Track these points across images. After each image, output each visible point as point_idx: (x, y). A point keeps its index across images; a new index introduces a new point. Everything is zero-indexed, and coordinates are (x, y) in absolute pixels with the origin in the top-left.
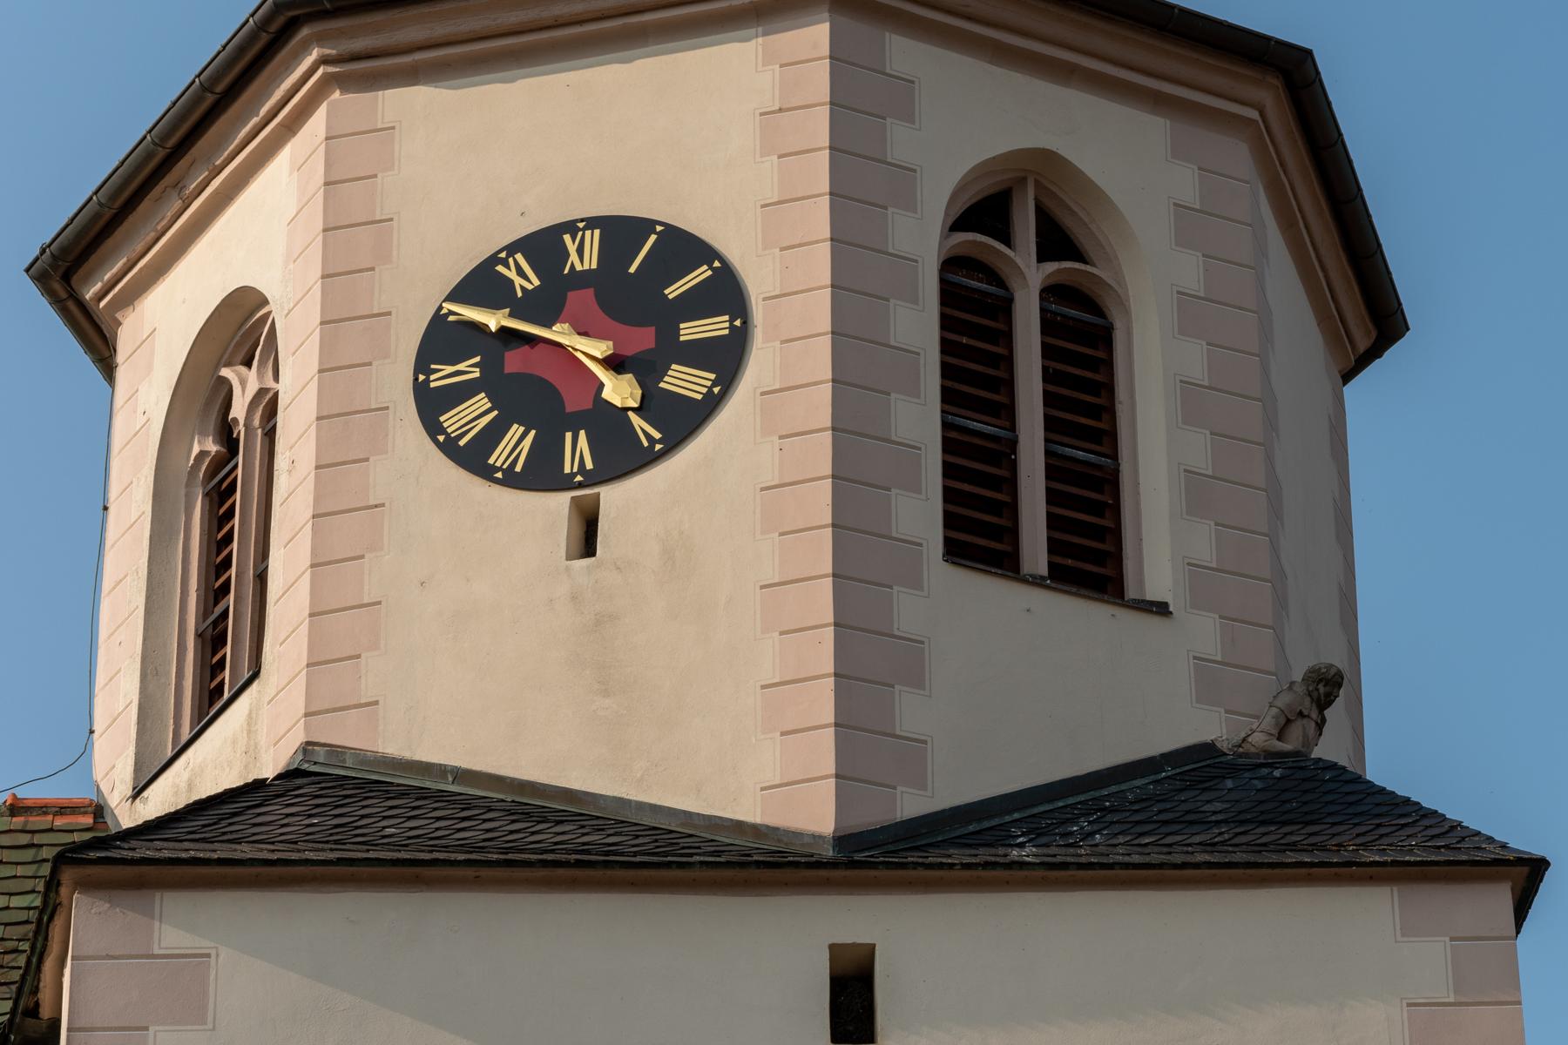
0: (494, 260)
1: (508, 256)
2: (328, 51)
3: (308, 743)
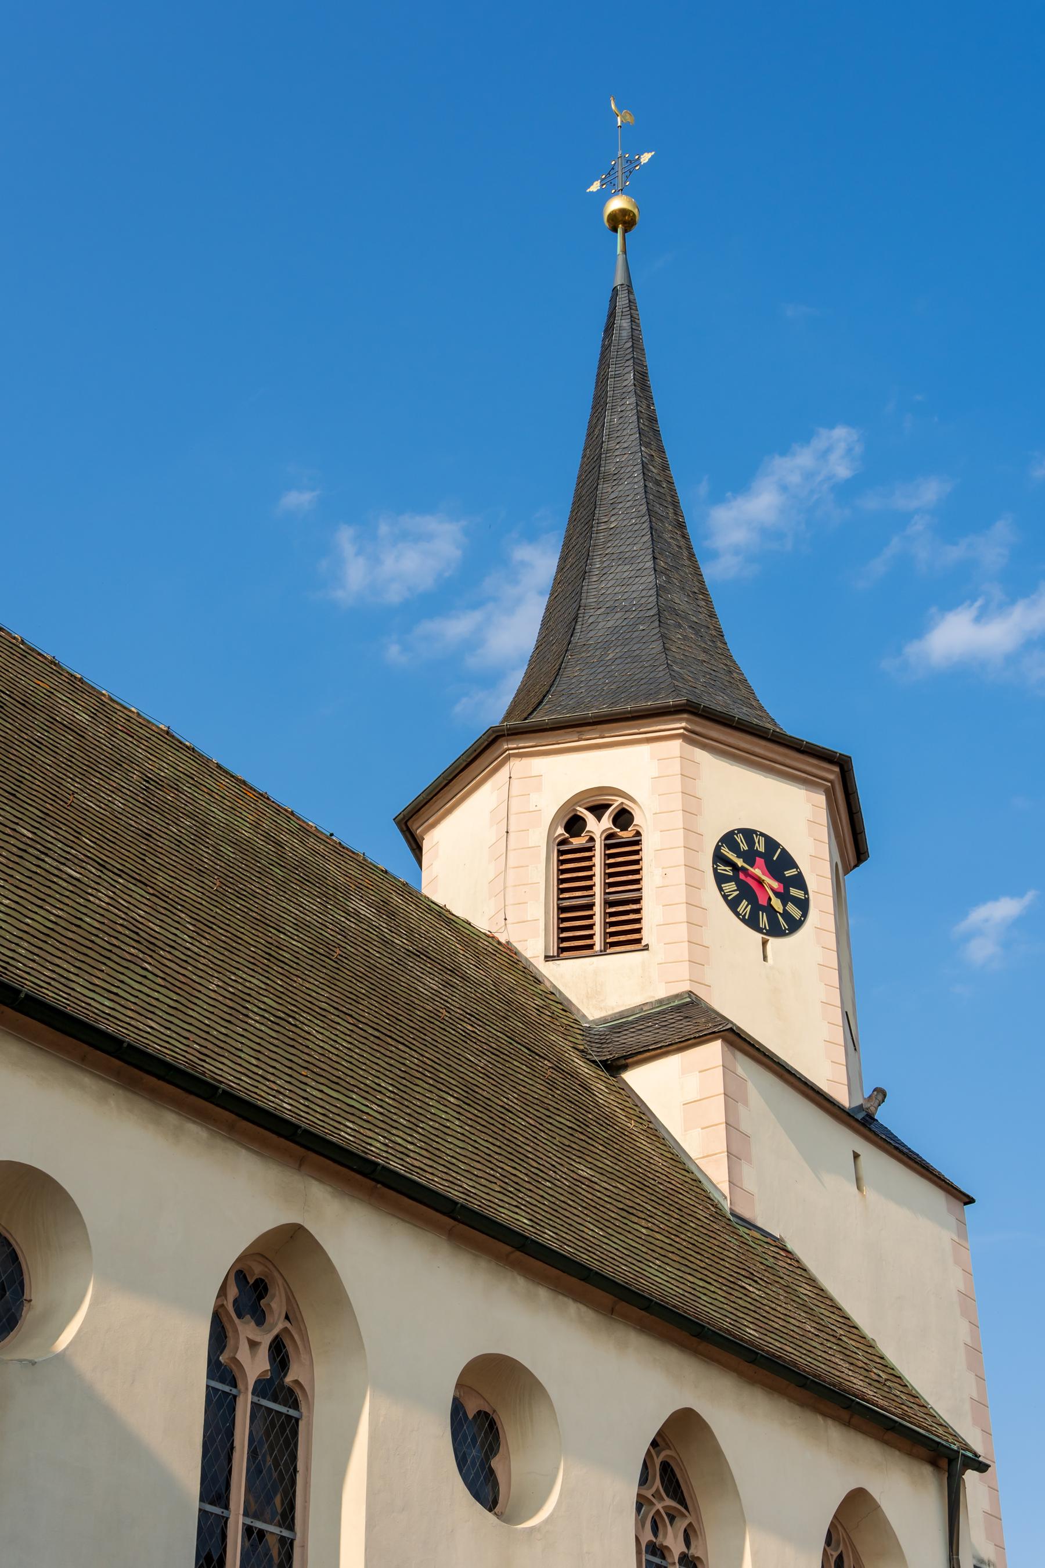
0: (743, 920)
1: (763, 929)
2: (688, 726)
3: (690, 991)
